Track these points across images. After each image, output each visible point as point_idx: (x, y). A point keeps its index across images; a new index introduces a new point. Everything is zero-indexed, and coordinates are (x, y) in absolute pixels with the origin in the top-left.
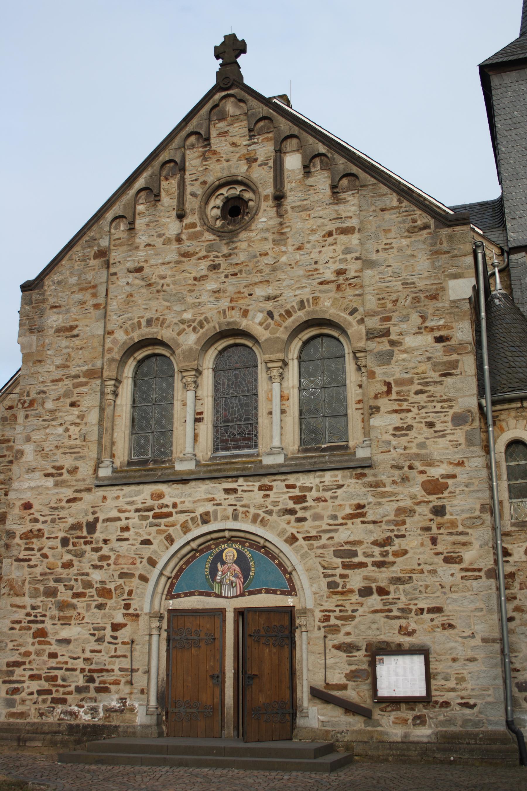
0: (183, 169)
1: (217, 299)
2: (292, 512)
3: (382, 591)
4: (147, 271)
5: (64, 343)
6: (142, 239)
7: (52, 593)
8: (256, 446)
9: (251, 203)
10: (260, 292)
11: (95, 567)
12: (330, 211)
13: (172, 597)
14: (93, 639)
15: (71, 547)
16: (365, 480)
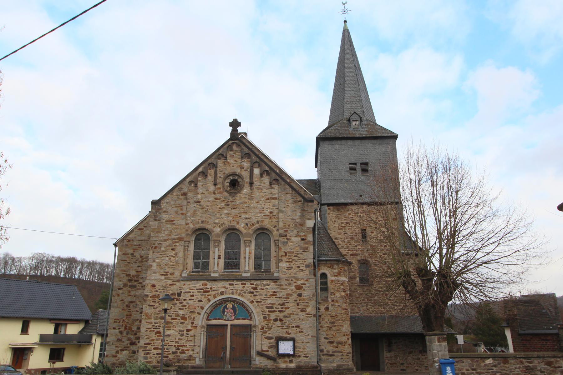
0: (217, 167)
2: (252, 293)
3: (281, 320)
4: (202, 203)
5: (169, 226)
6: (200, 191)
8: (239, 269)
10: (243, 216)
11: (180, 309)
12: (269, 191)
13: (209, 320)
14: (179, 335)
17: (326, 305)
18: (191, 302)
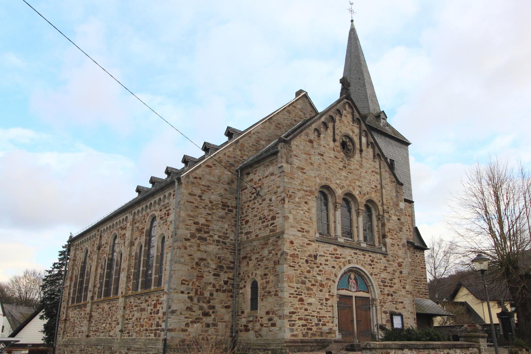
3: (392, 295)
4: (324, 157)
10: (358, 183)
14: (319, 304)
15: (309, 264)
18: (326, 268)
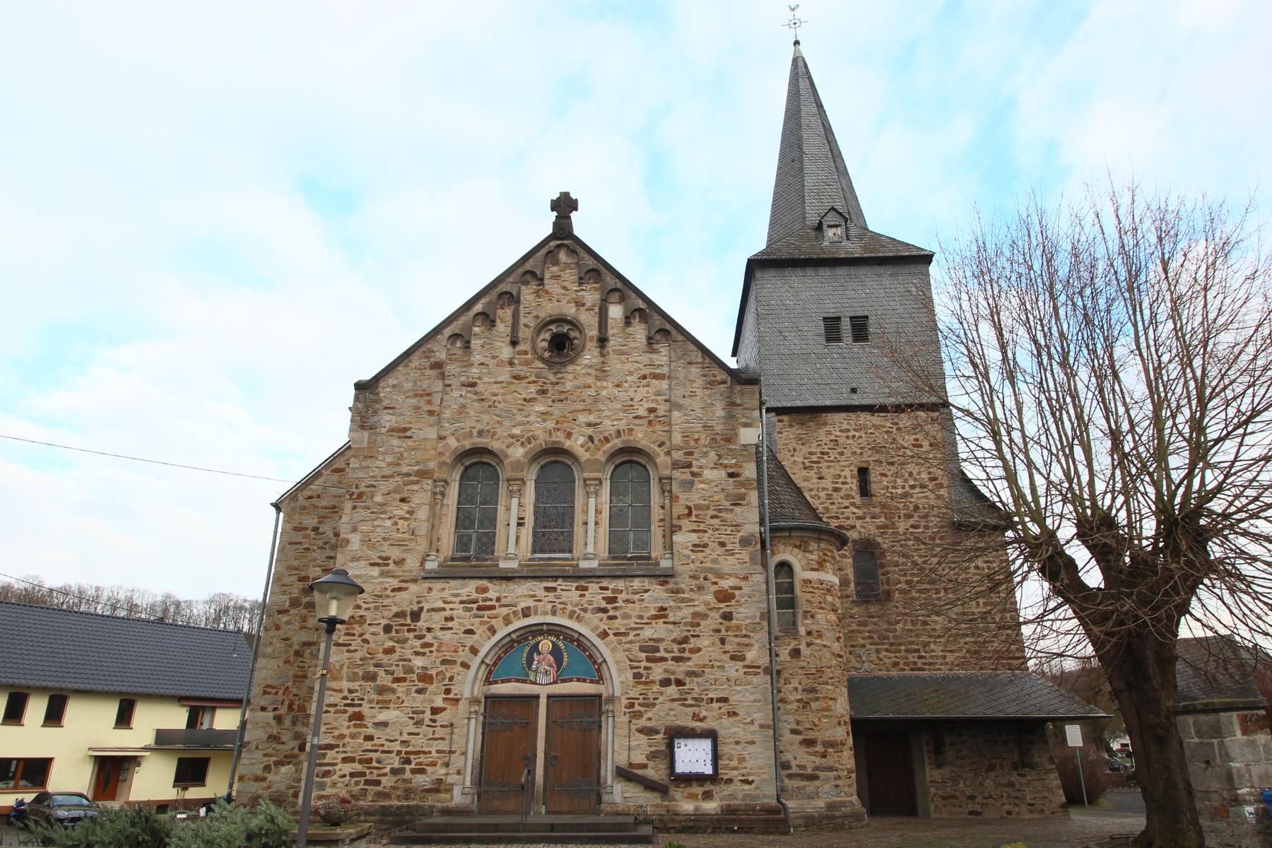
0: (518, 302)
1: (544, 420)
2: (604, 610)
3: (679, 683)
4: (480, 388)
5: (396, 442)
6: (477, 358)
7: (372, 677)
8: (570, 551)
9: (576, 342)
10: (583, 418)
11: (417, 653)
12: (645, 359)
13: (490, 683)
14: (411, 722)
15: (393, 634)
16: (669, 586)
17: (793, 644)
18: (447, 636)
